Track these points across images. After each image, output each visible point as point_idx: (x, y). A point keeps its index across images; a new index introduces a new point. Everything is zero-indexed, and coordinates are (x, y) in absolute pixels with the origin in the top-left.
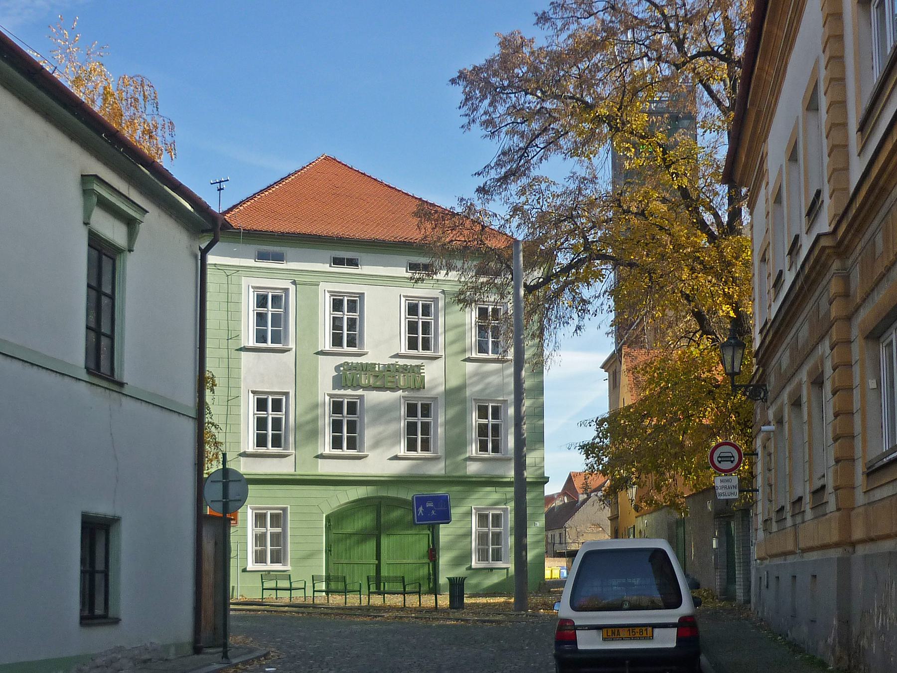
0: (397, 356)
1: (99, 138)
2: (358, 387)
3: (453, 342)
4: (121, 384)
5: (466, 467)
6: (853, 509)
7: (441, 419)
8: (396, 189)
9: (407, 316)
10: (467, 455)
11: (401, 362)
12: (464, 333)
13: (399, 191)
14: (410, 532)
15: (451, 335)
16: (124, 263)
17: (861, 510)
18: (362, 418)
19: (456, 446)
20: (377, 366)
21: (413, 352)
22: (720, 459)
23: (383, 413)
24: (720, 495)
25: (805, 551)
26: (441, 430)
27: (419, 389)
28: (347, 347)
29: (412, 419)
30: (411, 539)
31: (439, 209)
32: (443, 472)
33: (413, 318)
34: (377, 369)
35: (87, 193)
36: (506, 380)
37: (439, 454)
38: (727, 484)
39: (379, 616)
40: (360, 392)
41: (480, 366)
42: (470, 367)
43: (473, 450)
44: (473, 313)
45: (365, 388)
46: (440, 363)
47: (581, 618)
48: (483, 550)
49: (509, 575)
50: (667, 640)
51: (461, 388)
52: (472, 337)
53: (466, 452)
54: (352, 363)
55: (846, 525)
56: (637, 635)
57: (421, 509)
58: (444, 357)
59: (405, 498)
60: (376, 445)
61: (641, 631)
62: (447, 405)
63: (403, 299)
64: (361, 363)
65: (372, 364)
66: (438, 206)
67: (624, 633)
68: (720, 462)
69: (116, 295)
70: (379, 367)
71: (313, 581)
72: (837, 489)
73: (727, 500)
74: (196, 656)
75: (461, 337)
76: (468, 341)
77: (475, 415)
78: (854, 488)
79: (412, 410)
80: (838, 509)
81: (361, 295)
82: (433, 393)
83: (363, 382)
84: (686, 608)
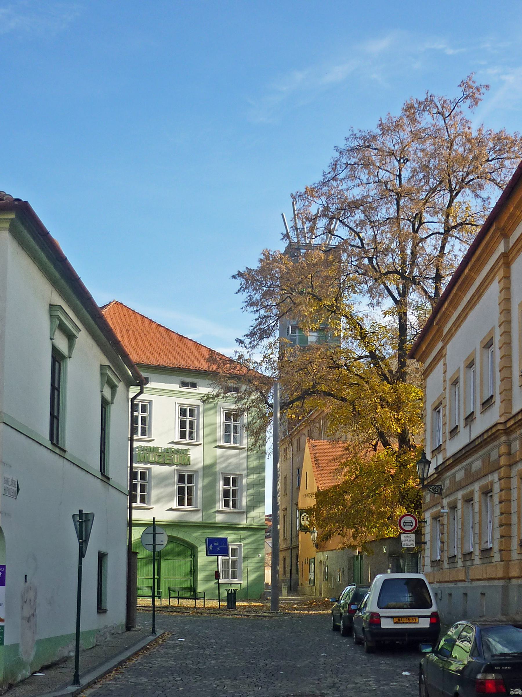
0: (173, 443)
1: (108, 343)
2: (148, 462)
3: (208, 435)
4: (108, 479)
5: (215, 517)
6: (510, 561)
7: (200, 485)
8: (165, 328)
9: (180, 417)
10: (217, 509)
11: (176, 447)
12: (215, 429)
13: (168, 329)
14: (179, 558)
15: (207, 430)
16: (110, 408)
17: (517, 562)
18: (149, 482)
19: (209, 503)
20: (160, 449)
21: (183, 441)
22: (404, 524)
23: (163, 479)
24: (404, 545)
25: (472, 580)
26: (200, 493)
27: (186, 465)
28: (141, 435)
29: (181, 485)
30: (180, 563)
31: (224, 358)
32: (200, 520)
33: (184, 418)
34: (160, 451)
35: (102, 374)
36: (241, 461)
37: (199, 508)
38: (408, 539)
39: (185, 612)
40: (149, 466)
41: (225, 452)
42: (219, 451)
43: (220, 506)
44: (222, 415)
45: (152, 463)
46: (200, 448)
47: (383, 612)
48: (225, 571)
49: (242, 588)
50: (425, 624)
51: (212, 466)
52: (220, 432)
53: (215, 507)
54: (144, 446)
55: (507, 568)
56: (411, 621)
57: (211, 546)
58: (202, 444)
59: (177, 536)
60: (158, 500)
61: (413, 620)
62: (204, 476)
63: (177, 405)
64: (150, 447)
65: (157, 447)
66: (222, 355)
67: (404, 620)
68: (404, 526)
69: (60, 416)
70: (161, 450)
71: (169, 591)
72: (500, 551)
73: (408, 548)
74: (128, 632)
75: (214, 432)
76: (218, 434)
77: (221, 483)
78: (510, 551)
79: (181, 478)
80: (502, 561)
81: (150, 402)
82: (195, 468)
83: (151, 459)
84: (434, 609)
